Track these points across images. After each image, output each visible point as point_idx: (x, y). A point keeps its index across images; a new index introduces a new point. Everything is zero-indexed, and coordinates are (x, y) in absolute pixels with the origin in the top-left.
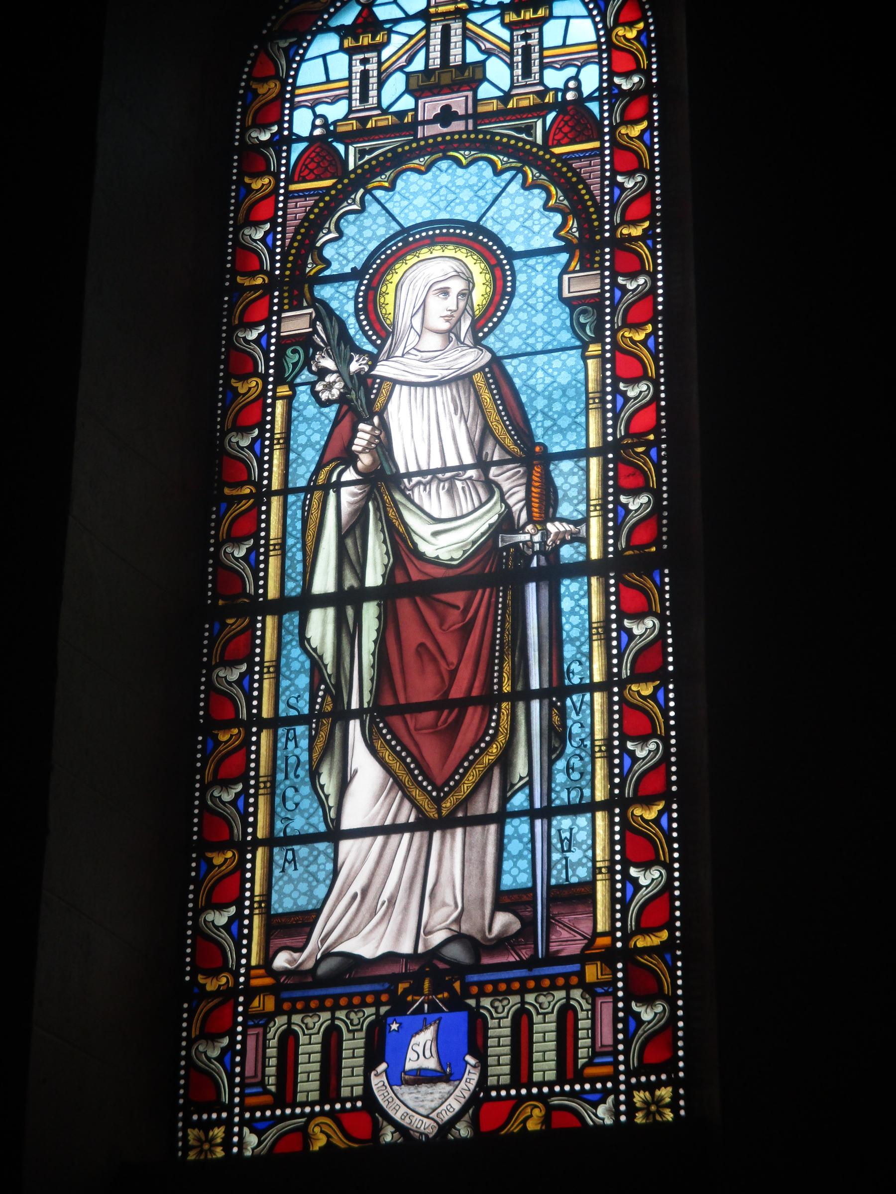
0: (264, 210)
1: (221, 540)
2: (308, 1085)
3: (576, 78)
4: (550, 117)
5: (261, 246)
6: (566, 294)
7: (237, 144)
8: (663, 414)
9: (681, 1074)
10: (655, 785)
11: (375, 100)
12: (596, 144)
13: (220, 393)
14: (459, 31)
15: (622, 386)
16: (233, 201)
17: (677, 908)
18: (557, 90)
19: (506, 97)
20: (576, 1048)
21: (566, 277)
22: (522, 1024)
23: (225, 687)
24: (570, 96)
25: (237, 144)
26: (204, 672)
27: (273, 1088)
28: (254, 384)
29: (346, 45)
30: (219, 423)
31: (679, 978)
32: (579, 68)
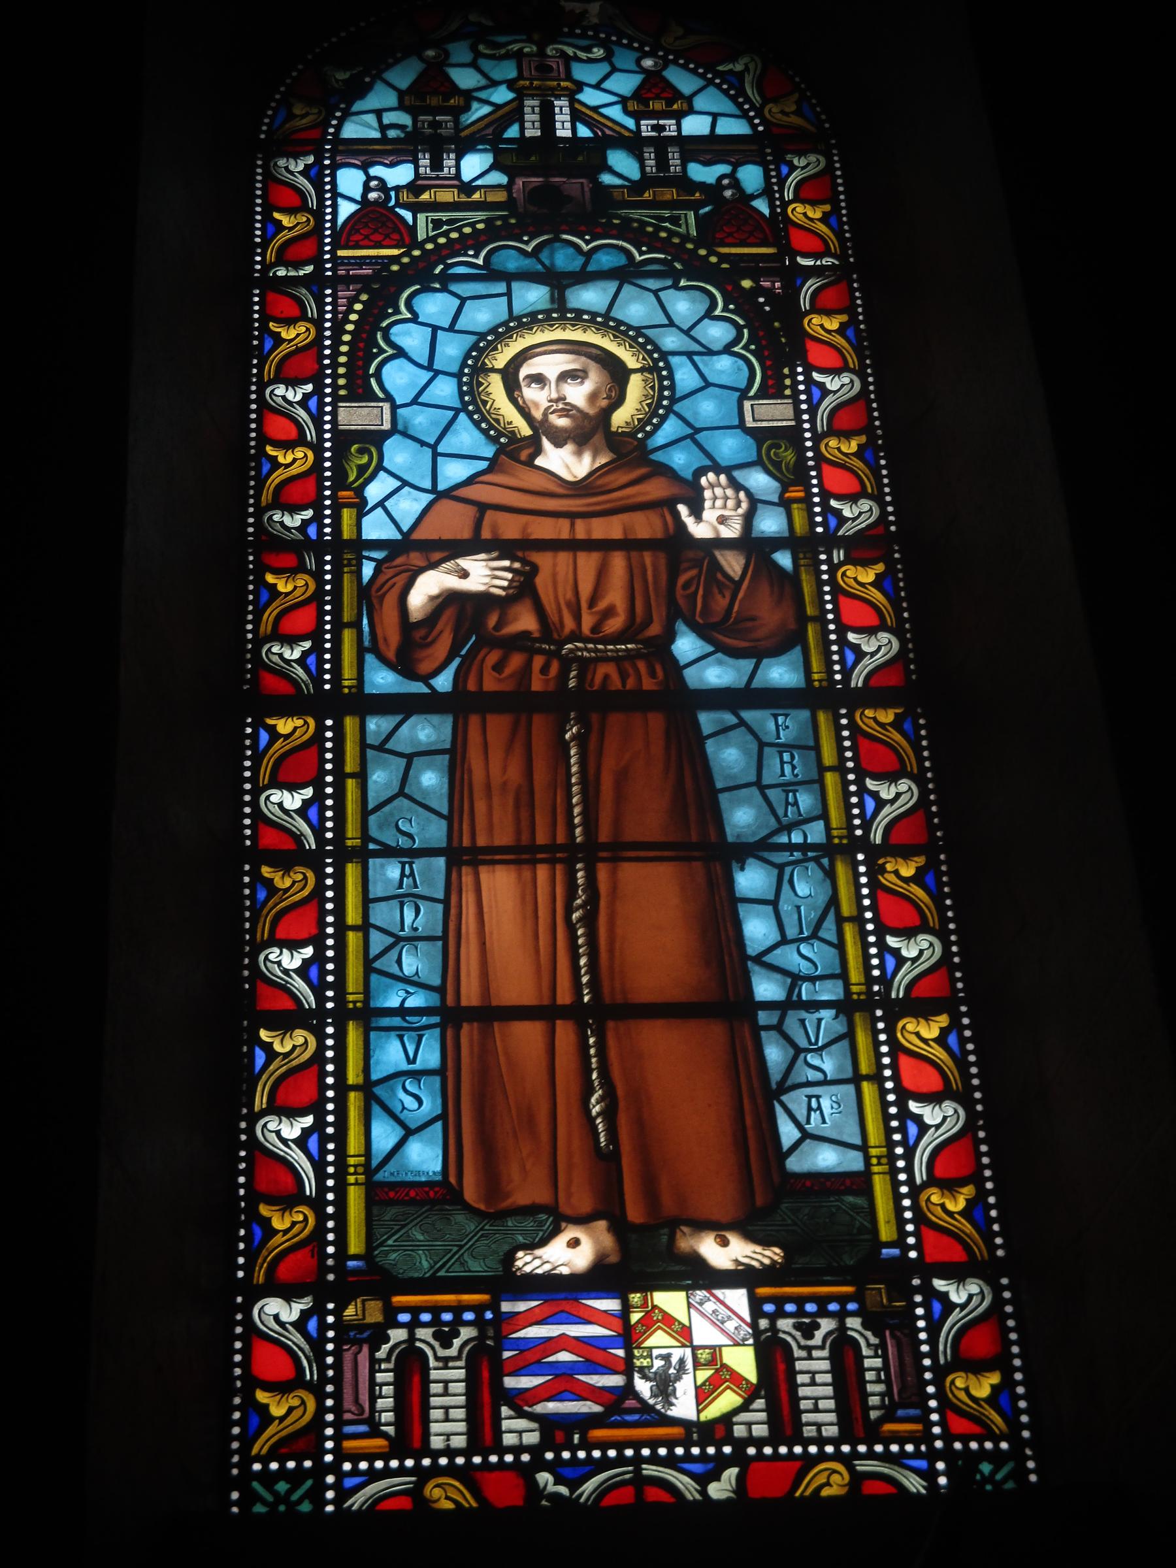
1: (257, 1109)
3: (732, 176)
5: (302, 413)
6: (750, 423)
7: (263, 136)
8: (958, 975)
9: (1033, 1478)
10: (981, 1344)
11: (453, 171)
13: (251, 592)
14: (566, 110)
15: (833, 503)
16: (236, 1430)
17: (901, 580)
21: (747, 405)
23: (280, 1149)
25: (235, 1471)
26: (247, 867)
27: (390, 1430)
28: (301, 455)
29: (407, 103)
30: (247, 931)
31: (926, 759)
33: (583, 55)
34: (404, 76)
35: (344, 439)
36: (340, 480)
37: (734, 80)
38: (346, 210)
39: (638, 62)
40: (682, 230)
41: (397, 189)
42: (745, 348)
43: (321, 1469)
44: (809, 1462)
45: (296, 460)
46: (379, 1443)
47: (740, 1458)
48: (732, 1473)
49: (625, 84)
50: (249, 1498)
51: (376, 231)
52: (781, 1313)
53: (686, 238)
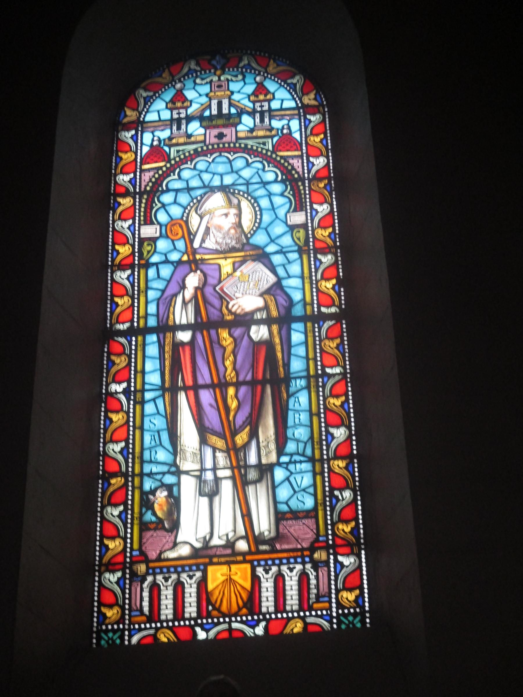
0: (119, 497)
2: (167, 610)
3: (288, 125)
4: (275, 139)
10: (344, 451)
12: (299, 153)
18: (278, 129)
19: (252, 130)
20: (309, 593)
22: (279, 579)
24: (285, 131)
29: (169, 106)
32: (289, 121)
33: (234, 79)
34: (169, 95)
35: (142, 241)
36: (141, 257)
37: (292, 86)
38: (146, 149)
39: (255, 79)
40: (267, 147)
41: (164, 140)
42: (289, 193)
43: (124, 630)
44: (289, 619)
45: (124, 250)
46: (144, 618)
47: (265, 619)
48: (263, 624)
49: (250, 89)
50: (99, 639)
51: (156, 156)
52: (281, 563)
53: (267, 150)
